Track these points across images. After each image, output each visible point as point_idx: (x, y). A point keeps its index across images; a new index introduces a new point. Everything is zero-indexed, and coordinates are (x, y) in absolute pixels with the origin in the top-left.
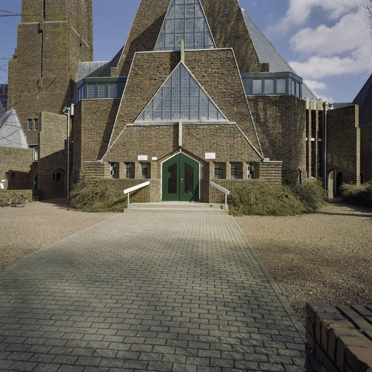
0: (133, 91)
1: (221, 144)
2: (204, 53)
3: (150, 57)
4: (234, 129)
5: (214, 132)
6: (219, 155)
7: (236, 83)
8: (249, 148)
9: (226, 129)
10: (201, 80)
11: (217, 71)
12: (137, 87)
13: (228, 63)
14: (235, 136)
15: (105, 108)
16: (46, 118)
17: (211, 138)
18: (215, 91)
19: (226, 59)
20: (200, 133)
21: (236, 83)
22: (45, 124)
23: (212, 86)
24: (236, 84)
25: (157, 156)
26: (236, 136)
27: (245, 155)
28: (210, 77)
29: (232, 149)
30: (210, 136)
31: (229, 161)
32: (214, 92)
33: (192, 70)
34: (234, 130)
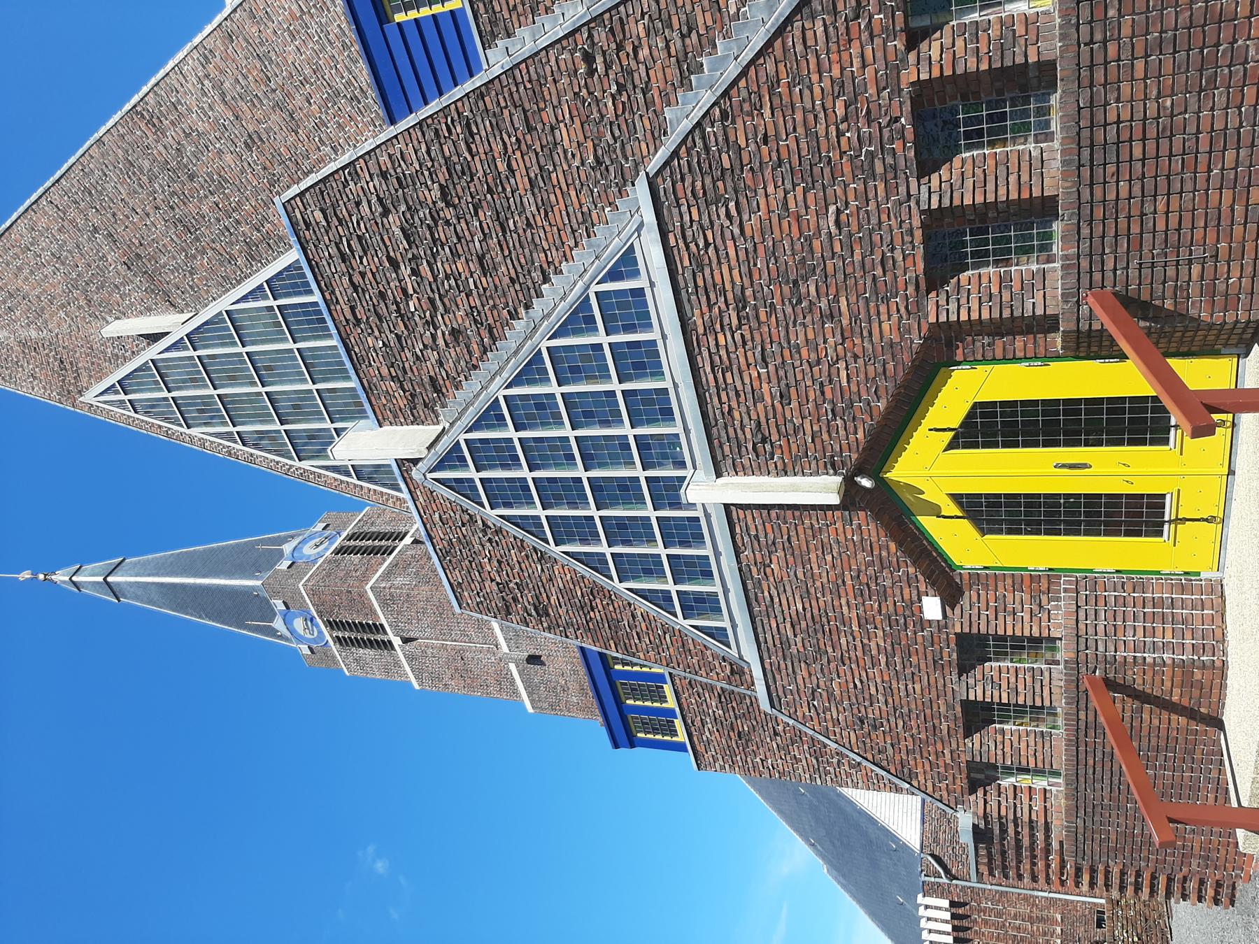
1: (798, 247)
2: (353, 340)
3: (454, 560)
4: (683, 180)
5: (723, 307)
6: (877, 257)
7: (429, 154)
8: (799, 48)
9: (689, 233)
10: (475, 346)
11: (405, 271)
12: (593, 610)
13: (350, 216)
14: (727, 164)
17: (763, 317)
18: (504, 268)
19: (334, 229)
20: (747, 381)
21: (429, 154)
23: (485, 290)
24: (433, 154)
25: (915, 598)
26: (725, 156)
27: (857, 62)
28: (446, 300)
29: (816, 170)
30: (754, 324)
31: (913, 182)
32: (512, 271)
34: (688, 180)
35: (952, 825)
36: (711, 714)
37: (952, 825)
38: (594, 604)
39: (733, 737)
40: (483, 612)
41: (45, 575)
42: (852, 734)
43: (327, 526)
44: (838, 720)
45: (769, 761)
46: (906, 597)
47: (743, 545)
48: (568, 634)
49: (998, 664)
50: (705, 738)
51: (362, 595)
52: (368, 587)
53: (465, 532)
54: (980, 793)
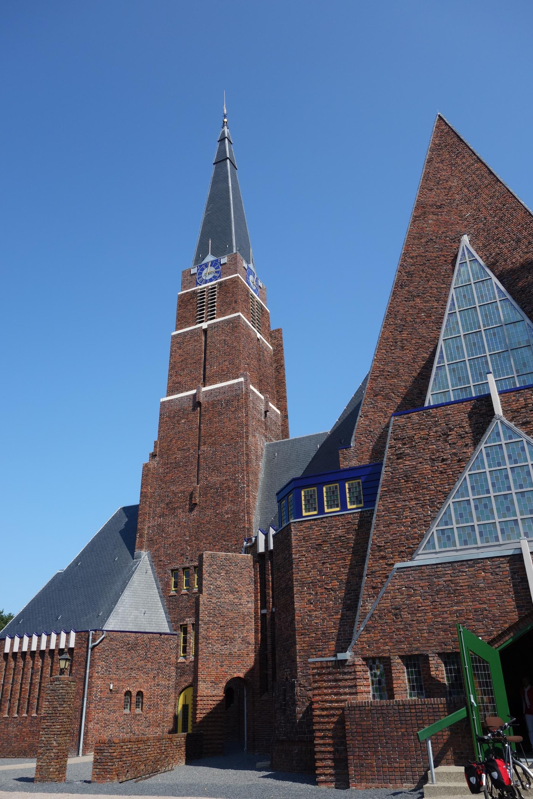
0: (398, 491)
12: (405, 481)
15: (340, 532)
16: (211, 565)
22: (210, 579)
33: (524, 427)
35: (120, 649)
36: (331, 532)
37: (120, 649)
38: (409, 482)
39: (318, 542)
40: (393, 427)
41: (226, 122)
42: (389, 605)
43: (261, 288)
44: (396, 598)
45: (304, 559)
46: (479, 631)
47: (493, 561)
48: (388, 468)
49: (444, 670)
50: (313, 527)
51: (238, 311)
52: (240, 314)
53: (442, 425)
54: (364, 663)
